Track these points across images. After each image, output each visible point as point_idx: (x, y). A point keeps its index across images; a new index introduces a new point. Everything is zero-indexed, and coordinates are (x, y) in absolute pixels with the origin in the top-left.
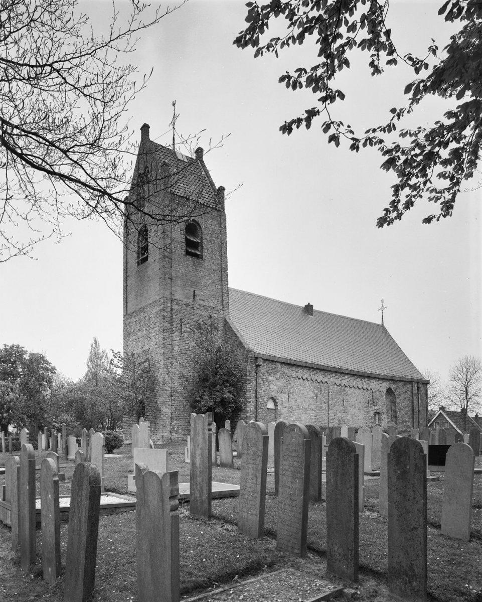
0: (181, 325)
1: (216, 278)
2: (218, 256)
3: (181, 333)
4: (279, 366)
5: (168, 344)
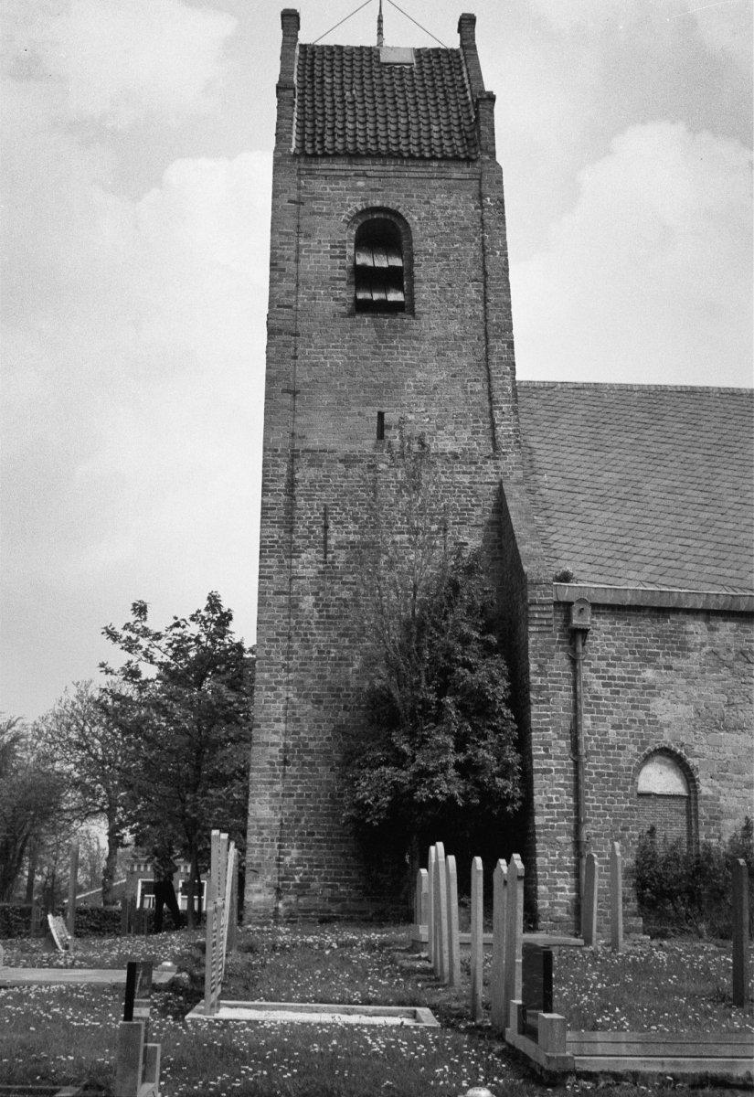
0: (326, 527)
1: (464, 362)
2: (472, 292)
3: (326, 553)
4: (696, 628)
5: (277, 593)
